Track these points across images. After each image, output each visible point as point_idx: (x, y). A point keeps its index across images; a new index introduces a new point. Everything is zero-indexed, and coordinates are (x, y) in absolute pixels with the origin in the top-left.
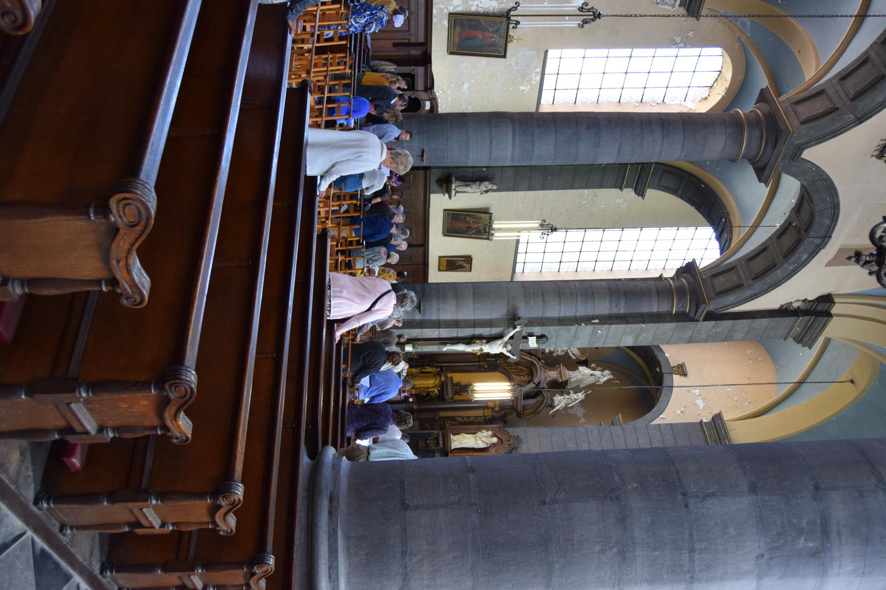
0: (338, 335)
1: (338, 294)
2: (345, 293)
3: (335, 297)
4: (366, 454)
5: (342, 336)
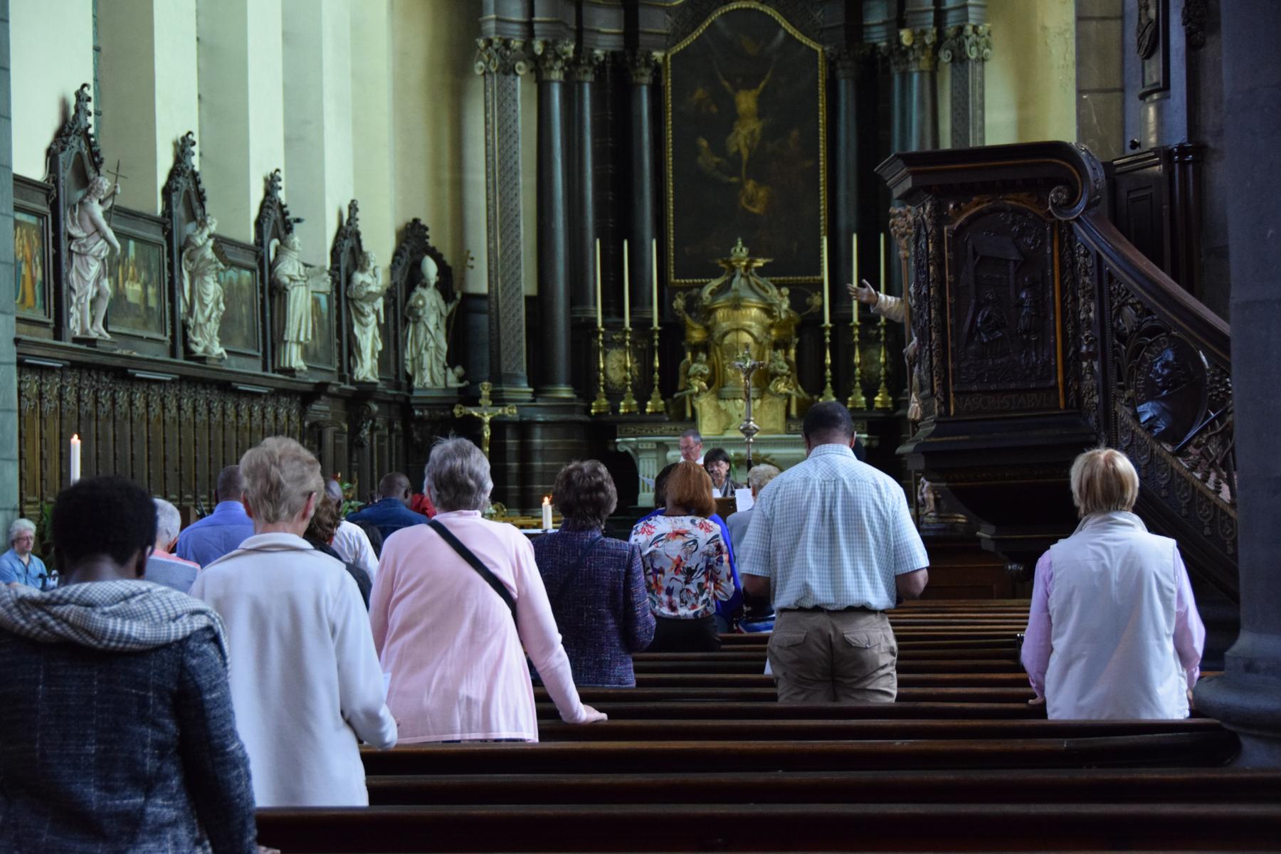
0: (587, 714)
1: (477, 715)
2: (473, 689)
3: (487, 724)
4: (819, 620)
5: (585, 699)
